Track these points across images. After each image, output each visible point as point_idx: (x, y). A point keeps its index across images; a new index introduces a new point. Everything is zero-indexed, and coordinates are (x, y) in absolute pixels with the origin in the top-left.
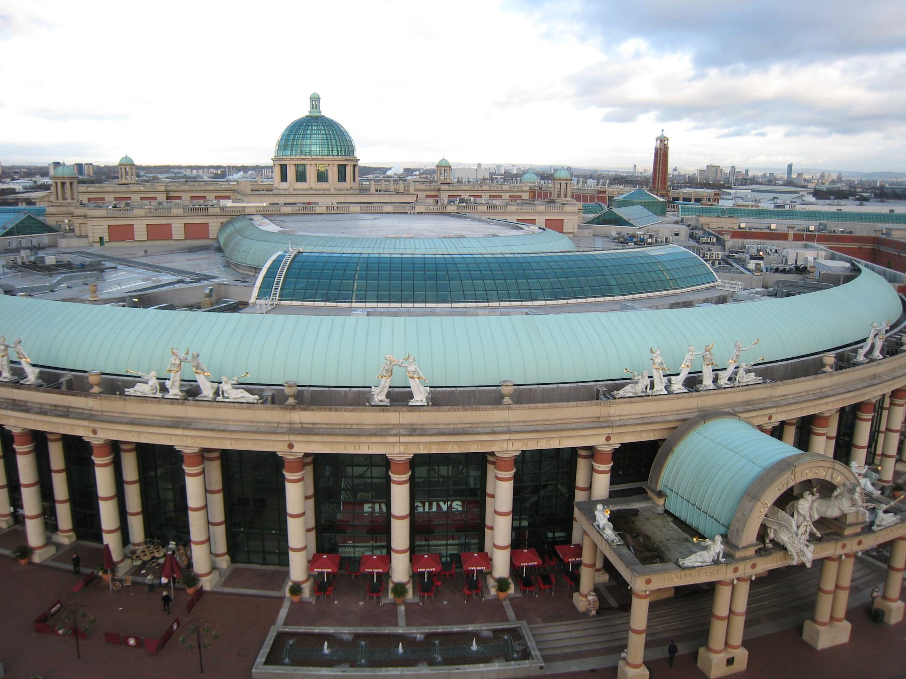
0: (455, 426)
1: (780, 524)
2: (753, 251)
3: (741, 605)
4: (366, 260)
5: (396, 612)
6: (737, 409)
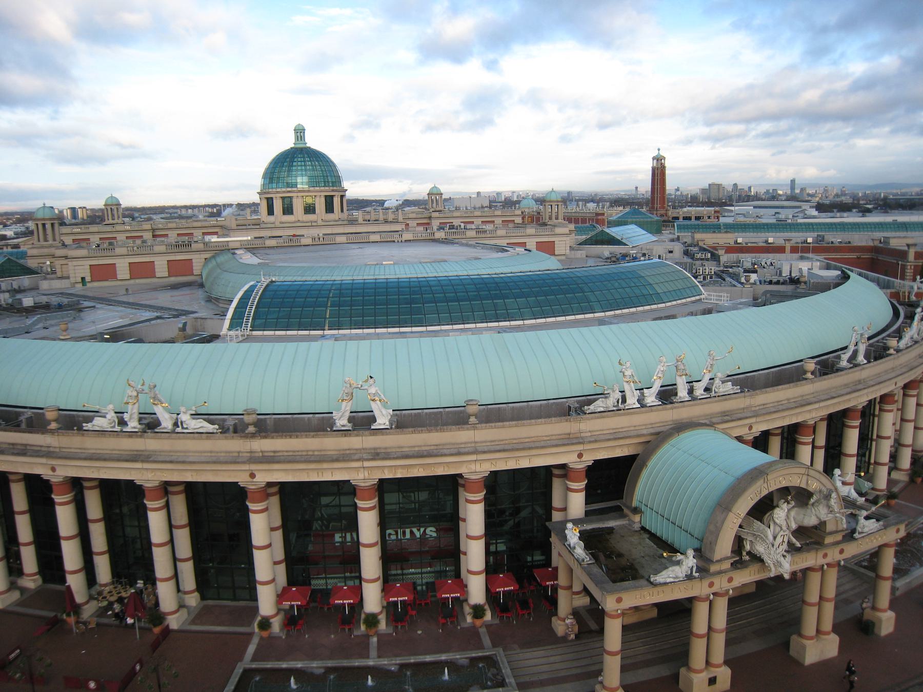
0: (420, 449)
1: (755, 535)
2: (748, 265)
3: (721, 621)
4: (339, 286)
5: (368, 644)
6: (714, 420)
